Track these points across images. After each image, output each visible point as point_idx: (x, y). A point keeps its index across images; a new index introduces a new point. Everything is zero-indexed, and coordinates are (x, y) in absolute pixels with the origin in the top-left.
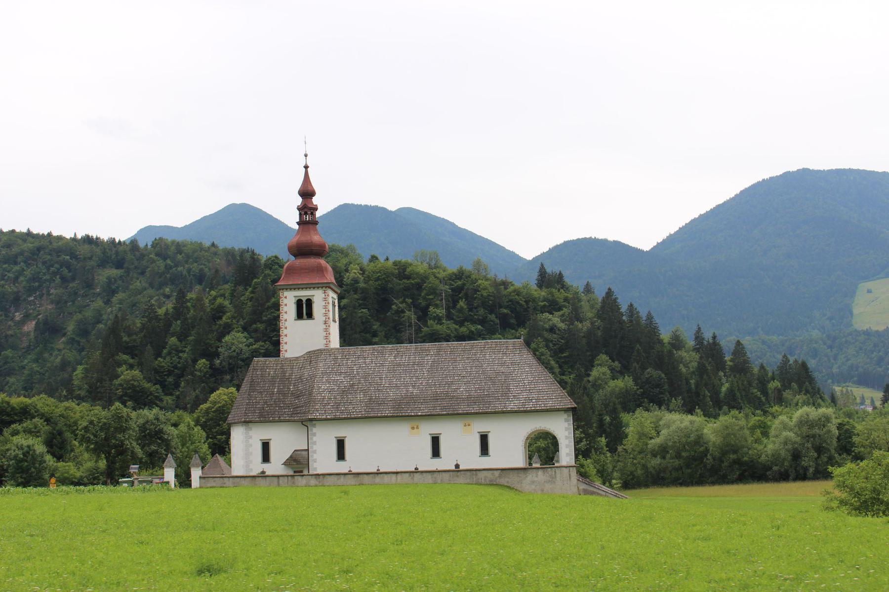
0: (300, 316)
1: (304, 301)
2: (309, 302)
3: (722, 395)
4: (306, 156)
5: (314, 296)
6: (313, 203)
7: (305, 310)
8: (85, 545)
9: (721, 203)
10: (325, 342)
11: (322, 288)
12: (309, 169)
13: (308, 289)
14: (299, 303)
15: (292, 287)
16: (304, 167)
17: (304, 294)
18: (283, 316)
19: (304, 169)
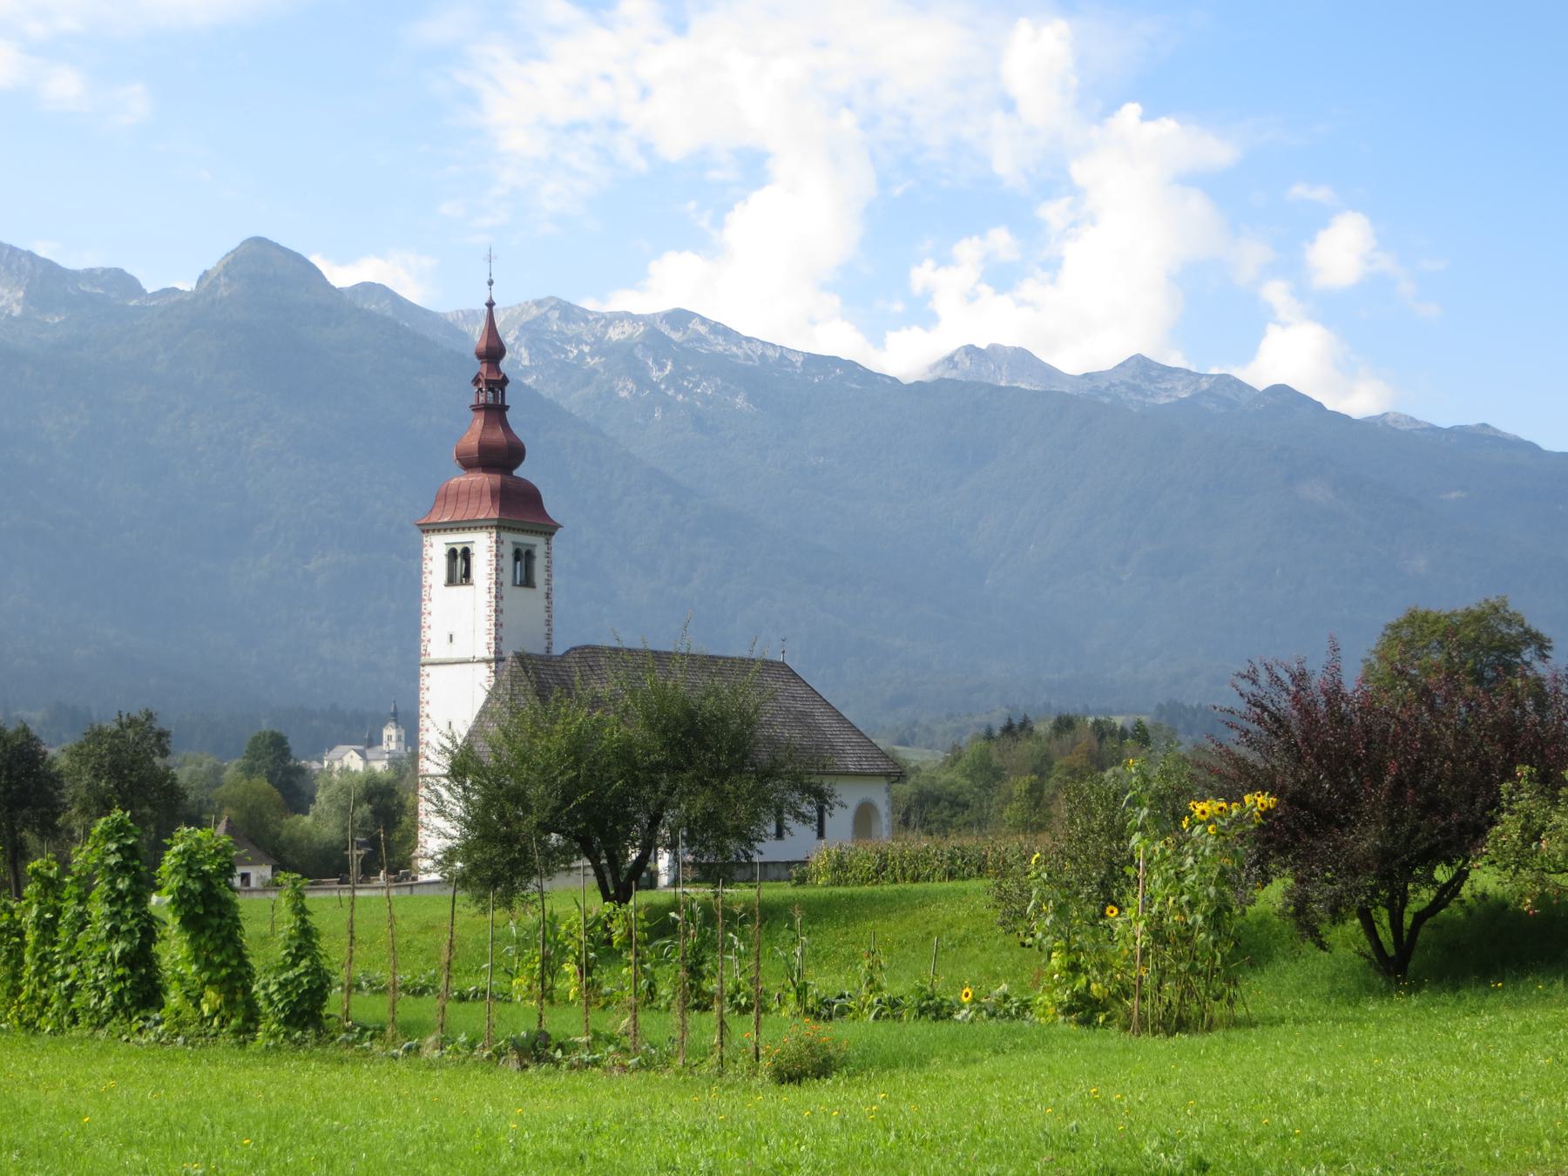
0: (451, 581)
1: (459, 551)
2: (466, 553)
3: (165, 841)
4: (491, 283)
5: (473, 542)
6: (144, 291)
7: (459, 567)
8: (1540, 822)
9: (332, 284)
10: (545, 643)
11: (487, 527)
12: (494, 307)
13: (461, 531)
14: (452, 554)
15: (459, 525)
16: (487, 304)
17: (458, 539)
18: (428, 580)
19: (486, 308)
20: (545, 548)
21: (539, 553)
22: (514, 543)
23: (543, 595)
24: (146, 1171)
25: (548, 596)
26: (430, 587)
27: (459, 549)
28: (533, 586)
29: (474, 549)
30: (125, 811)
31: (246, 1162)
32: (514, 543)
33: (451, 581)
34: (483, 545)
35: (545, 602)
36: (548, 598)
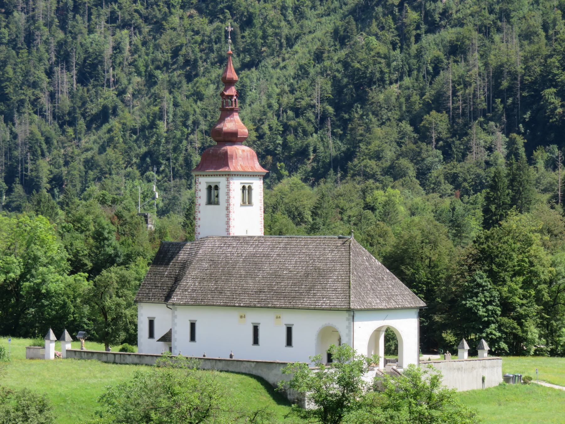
0: (244, 203)
1: (247, 188)
2: (217, 188)
14: (209, 188)
17: (246, 181)
20: (226, 183)
21: (222, 187)
22: (207, 183)
23: (225, 208)
24: (26, 418)
25: (227, 208)
26: (200, 205)
27: (247, 186)
28: (217, 203)
29: (253, 187)
30: (476, 335)
31: (191, 391)
32: (207, 183)
33: (244, 203)
34: (258, 185)
35: (226, 212)
36: (227, 209)
